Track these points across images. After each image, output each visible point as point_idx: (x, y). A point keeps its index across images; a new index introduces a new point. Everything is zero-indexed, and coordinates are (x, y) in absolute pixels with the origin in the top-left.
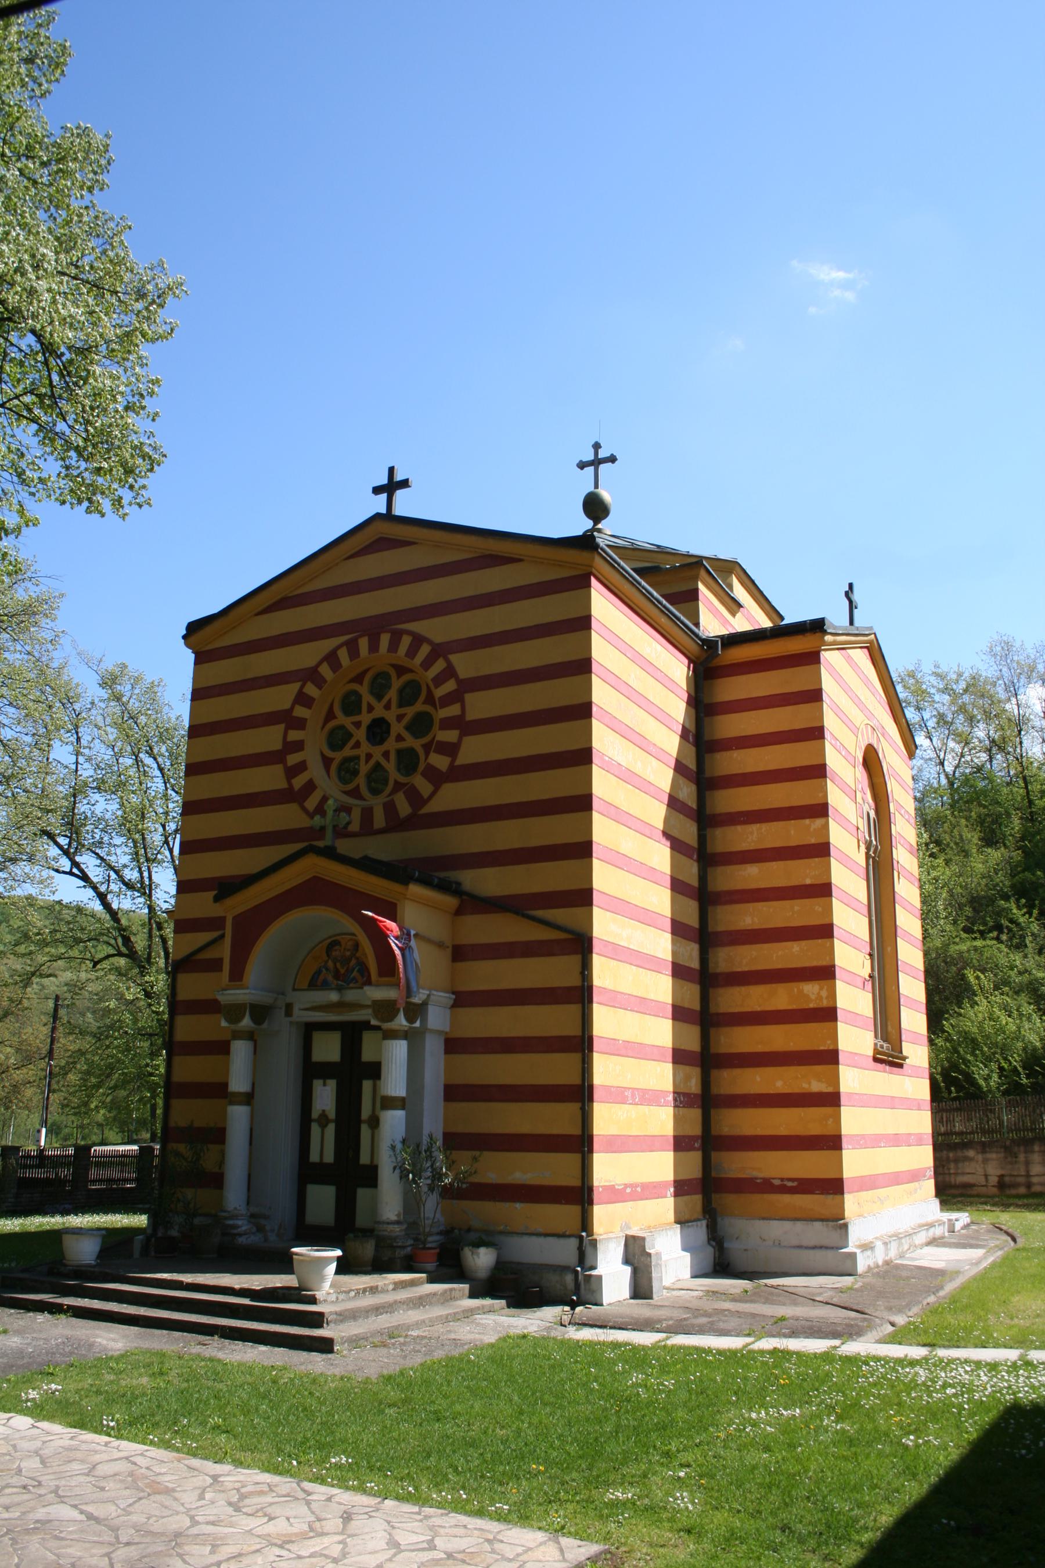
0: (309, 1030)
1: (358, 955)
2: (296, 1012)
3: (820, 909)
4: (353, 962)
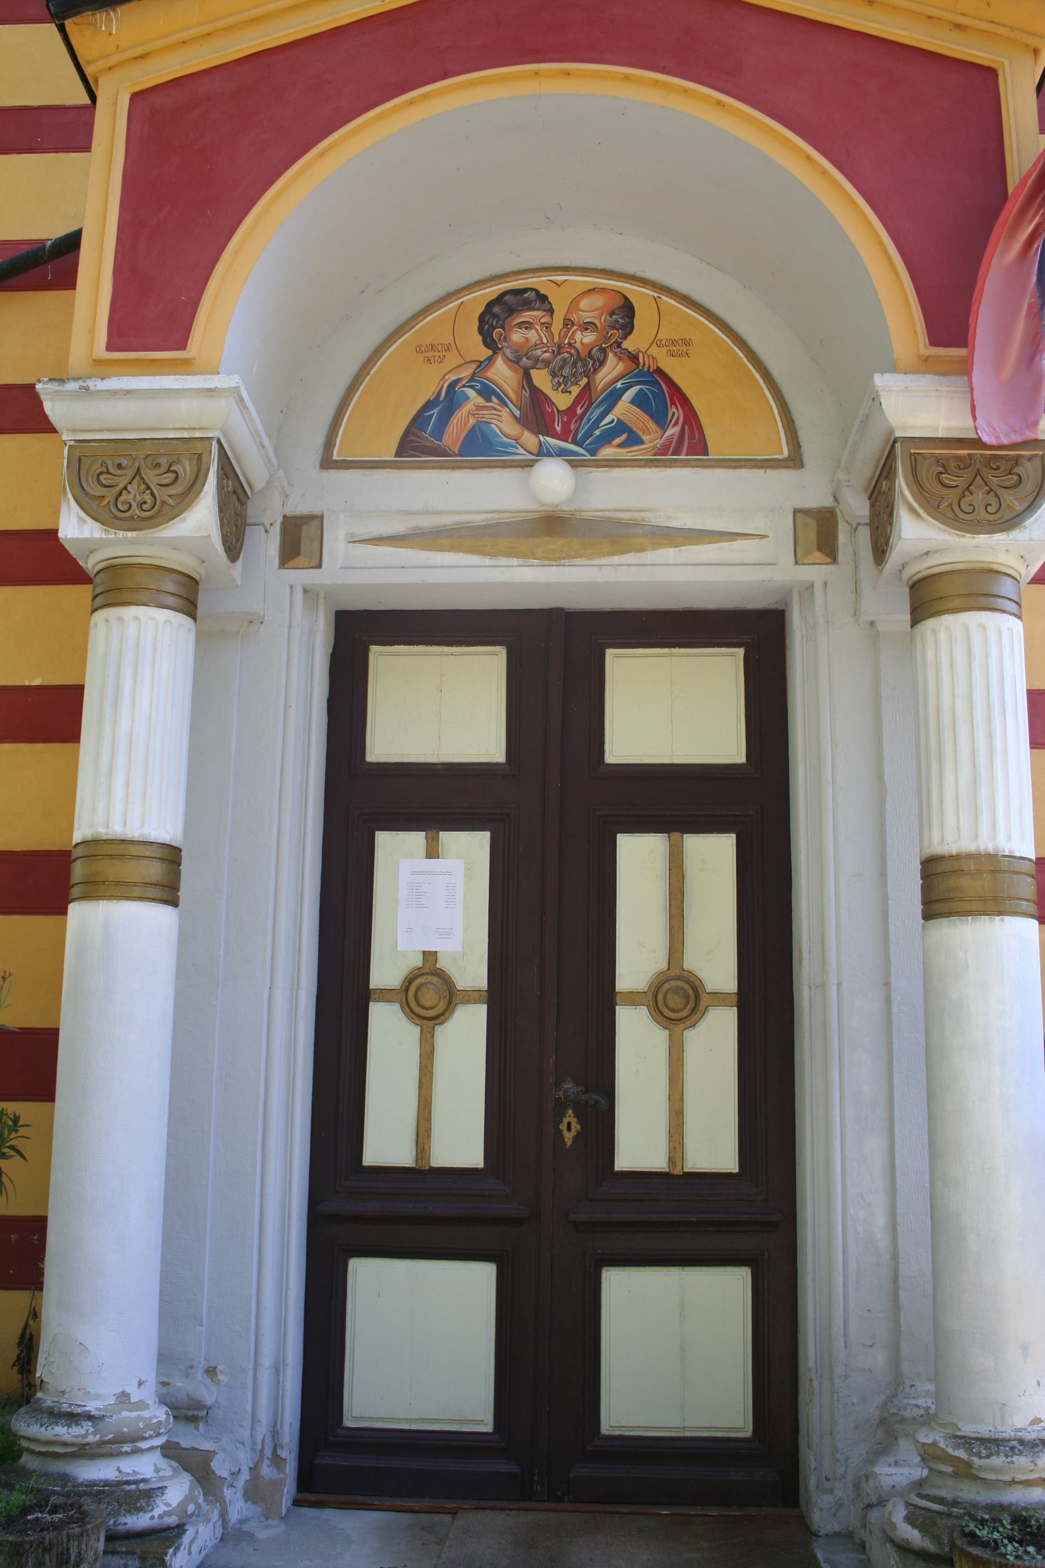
0: (358, 635)
1: (629, 344)
2: (336, 545)
4: (612, 369)
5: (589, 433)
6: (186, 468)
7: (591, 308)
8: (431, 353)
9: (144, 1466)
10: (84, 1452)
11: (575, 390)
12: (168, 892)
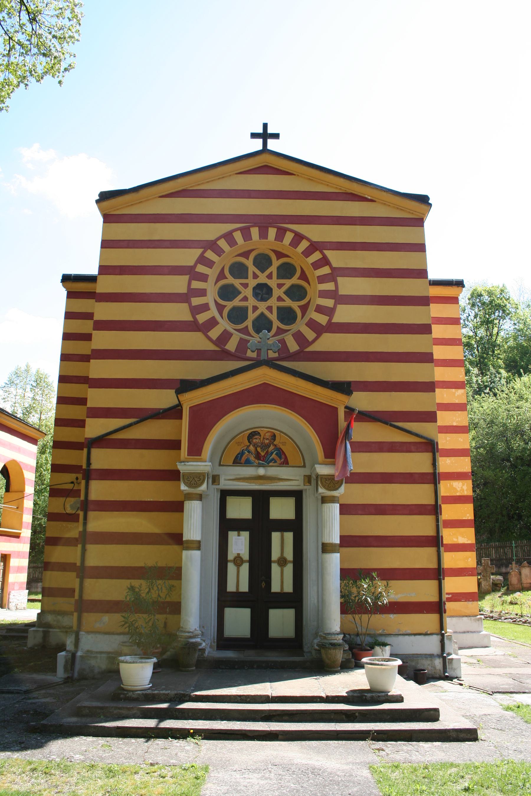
0: (225, 494)
1: (275, 443)
2: (222, 481)
3: (462, 440)
4: (272, 448)
5: (267, 460)
6: (202, 477)
7: (268, 435)
8: (239, 443)
9: (198, 640)
10: (191, 637)
11: (265, 452)
12: (199, 548)
